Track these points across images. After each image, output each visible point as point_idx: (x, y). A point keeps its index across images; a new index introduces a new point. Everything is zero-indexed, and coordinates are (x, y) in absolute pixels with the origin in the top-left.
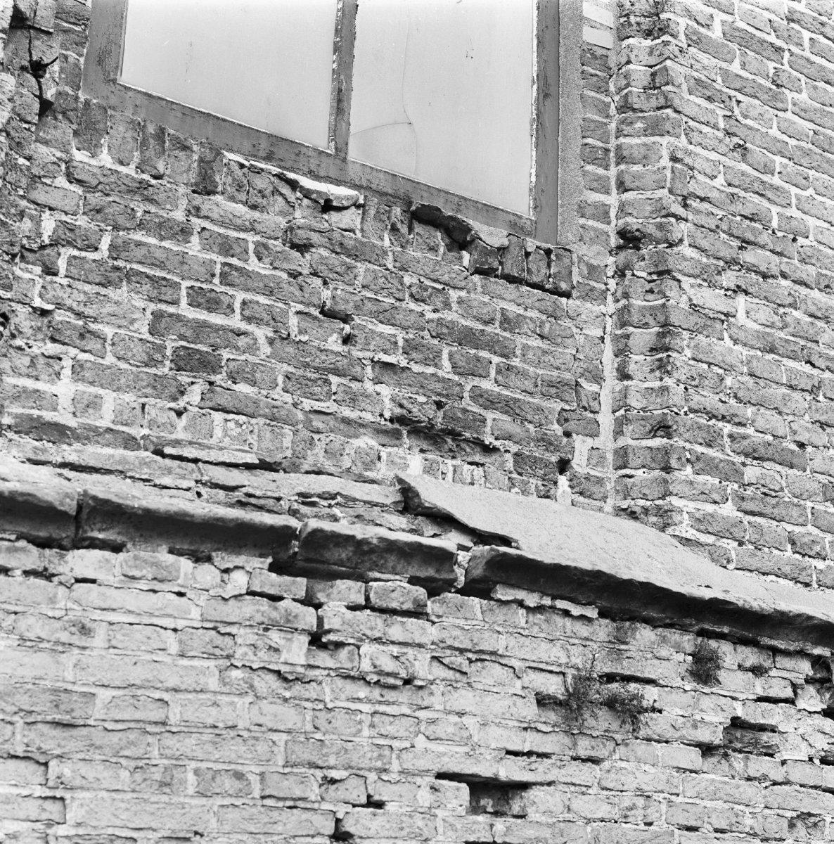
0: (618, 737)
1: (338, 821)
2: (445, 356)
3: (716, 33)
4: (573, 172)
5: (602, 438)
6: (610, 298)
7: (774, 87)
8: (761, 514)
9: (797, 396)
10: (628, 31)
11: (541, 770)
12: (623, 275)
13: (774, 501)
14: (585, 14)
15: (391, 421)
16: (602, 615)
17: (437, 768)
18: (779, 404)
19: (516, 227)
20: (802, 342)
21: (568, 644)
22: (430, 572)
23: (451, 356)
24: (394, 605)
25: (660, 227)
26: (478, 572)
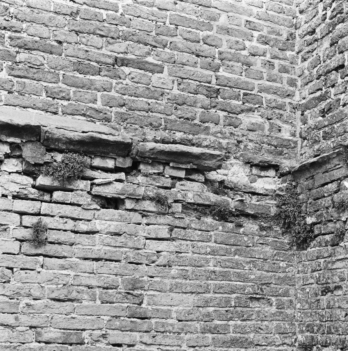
9: (60, 17)
18: (46, 21)
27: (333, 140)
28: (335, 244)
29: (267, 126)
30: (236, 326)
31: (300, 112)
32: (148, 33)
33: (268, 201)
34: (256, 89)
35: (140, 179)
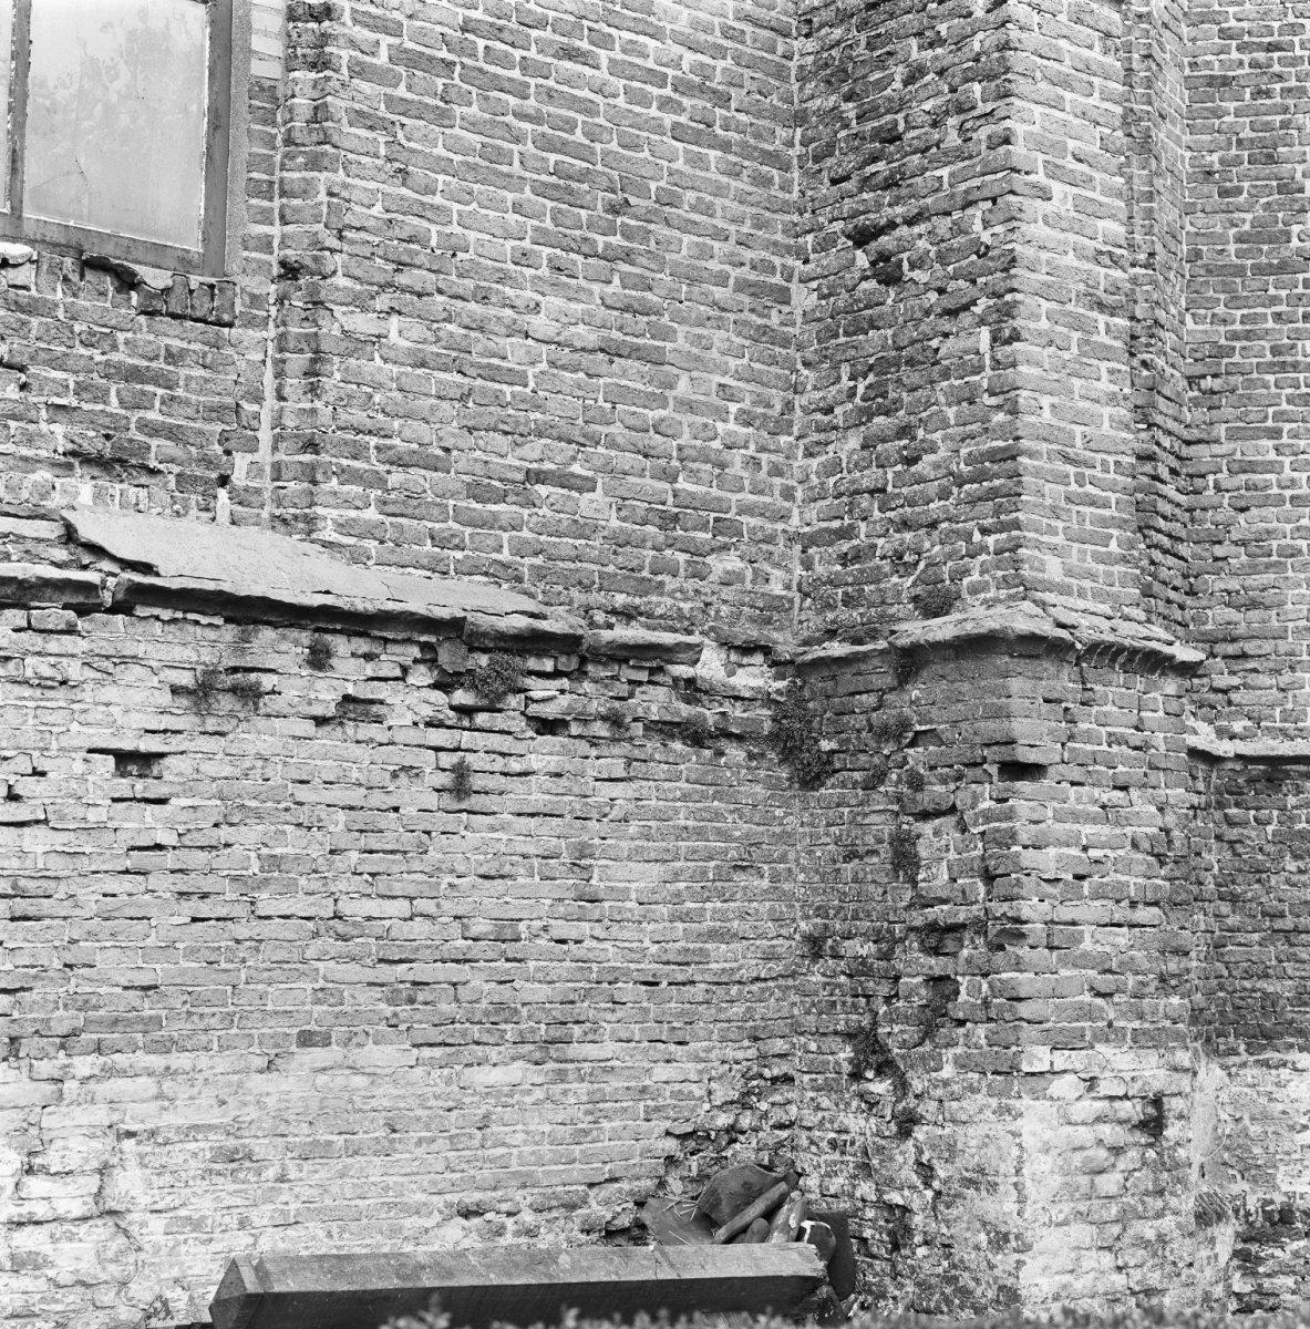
0: (241, 715)
1: (10, 787)
2: (113, 393)
3: (382, 59)
4: (240, 205)
5: (261, 452)
6: (271, 324)
7: (442, 104)
8: (402, 515)
9: (445, 405)
10: (294, 64)
11: (175, 743)
12: (282, 304)
13: (415, 502)
14: (254, 47)
15: (64, 454)
16: (228, 620)
17: (88, 745)
18: (426, 414)
19: (185, 264)
20: (454, 354)
21: (203, 645)
22: (81, 599)
23: (118, 392)
24: (50, 627)
25: (316, 259)
26: (120, 596)
27: (861, 610)
28: (869, 786)
29: (749, 575)
30: (715, 911)
31: (799, 547)
32: (572, 421)
33: (759, 711)
34: (734, 510)
35: (587, 686)
